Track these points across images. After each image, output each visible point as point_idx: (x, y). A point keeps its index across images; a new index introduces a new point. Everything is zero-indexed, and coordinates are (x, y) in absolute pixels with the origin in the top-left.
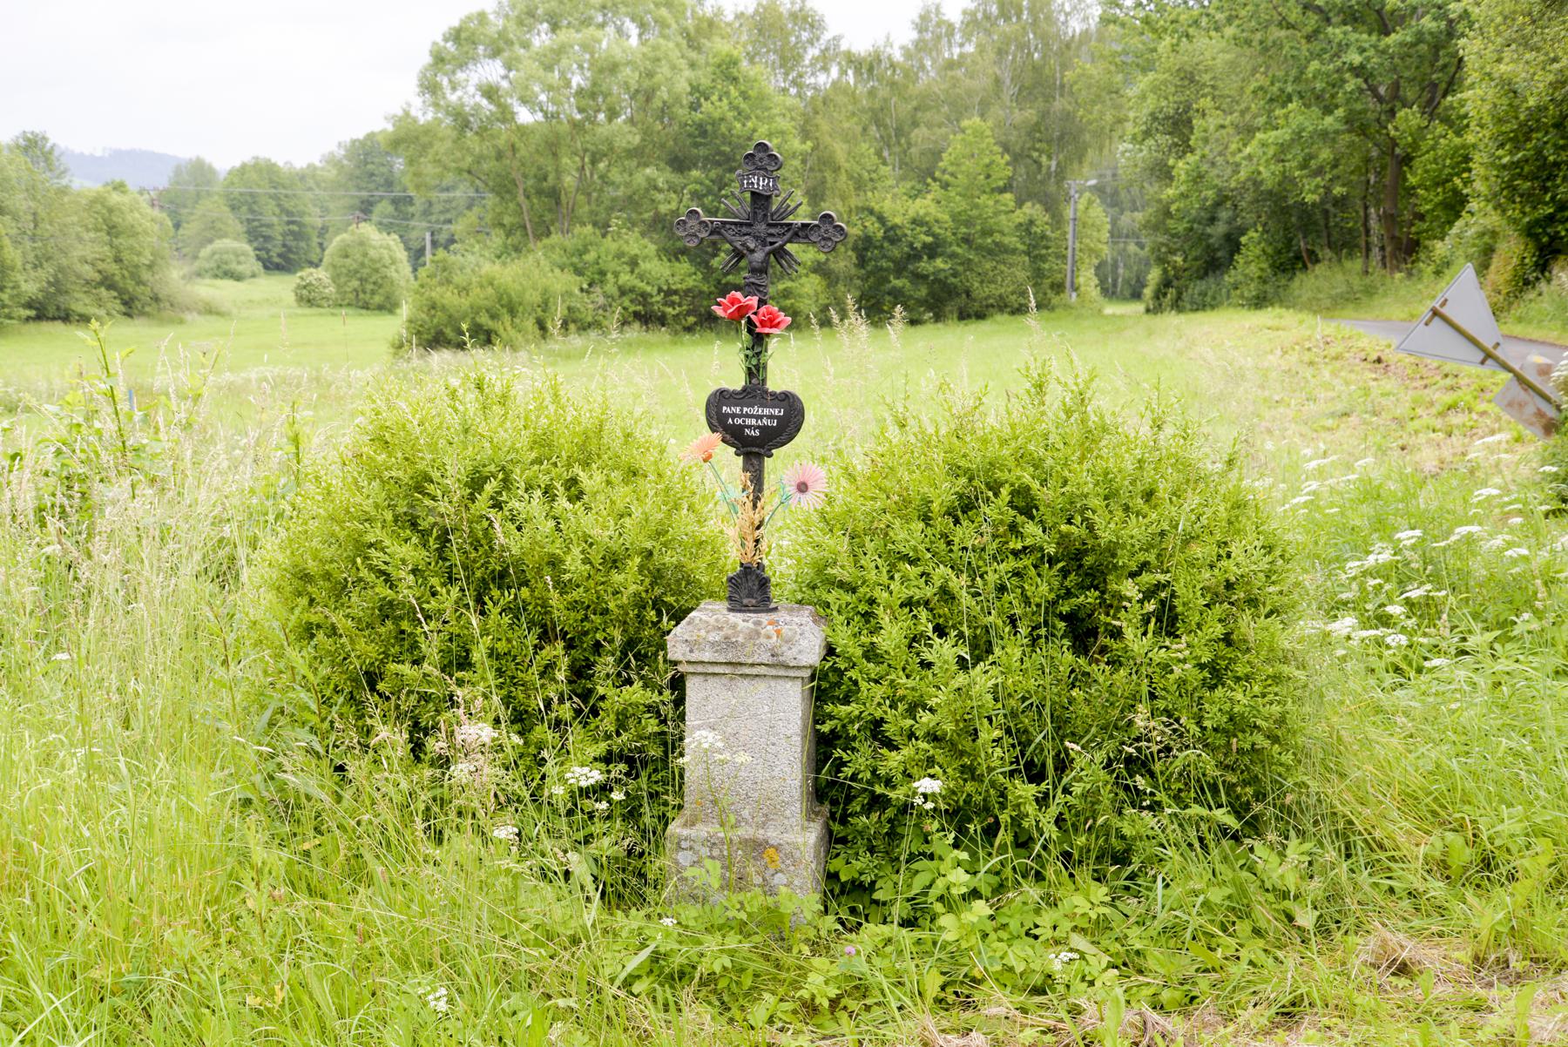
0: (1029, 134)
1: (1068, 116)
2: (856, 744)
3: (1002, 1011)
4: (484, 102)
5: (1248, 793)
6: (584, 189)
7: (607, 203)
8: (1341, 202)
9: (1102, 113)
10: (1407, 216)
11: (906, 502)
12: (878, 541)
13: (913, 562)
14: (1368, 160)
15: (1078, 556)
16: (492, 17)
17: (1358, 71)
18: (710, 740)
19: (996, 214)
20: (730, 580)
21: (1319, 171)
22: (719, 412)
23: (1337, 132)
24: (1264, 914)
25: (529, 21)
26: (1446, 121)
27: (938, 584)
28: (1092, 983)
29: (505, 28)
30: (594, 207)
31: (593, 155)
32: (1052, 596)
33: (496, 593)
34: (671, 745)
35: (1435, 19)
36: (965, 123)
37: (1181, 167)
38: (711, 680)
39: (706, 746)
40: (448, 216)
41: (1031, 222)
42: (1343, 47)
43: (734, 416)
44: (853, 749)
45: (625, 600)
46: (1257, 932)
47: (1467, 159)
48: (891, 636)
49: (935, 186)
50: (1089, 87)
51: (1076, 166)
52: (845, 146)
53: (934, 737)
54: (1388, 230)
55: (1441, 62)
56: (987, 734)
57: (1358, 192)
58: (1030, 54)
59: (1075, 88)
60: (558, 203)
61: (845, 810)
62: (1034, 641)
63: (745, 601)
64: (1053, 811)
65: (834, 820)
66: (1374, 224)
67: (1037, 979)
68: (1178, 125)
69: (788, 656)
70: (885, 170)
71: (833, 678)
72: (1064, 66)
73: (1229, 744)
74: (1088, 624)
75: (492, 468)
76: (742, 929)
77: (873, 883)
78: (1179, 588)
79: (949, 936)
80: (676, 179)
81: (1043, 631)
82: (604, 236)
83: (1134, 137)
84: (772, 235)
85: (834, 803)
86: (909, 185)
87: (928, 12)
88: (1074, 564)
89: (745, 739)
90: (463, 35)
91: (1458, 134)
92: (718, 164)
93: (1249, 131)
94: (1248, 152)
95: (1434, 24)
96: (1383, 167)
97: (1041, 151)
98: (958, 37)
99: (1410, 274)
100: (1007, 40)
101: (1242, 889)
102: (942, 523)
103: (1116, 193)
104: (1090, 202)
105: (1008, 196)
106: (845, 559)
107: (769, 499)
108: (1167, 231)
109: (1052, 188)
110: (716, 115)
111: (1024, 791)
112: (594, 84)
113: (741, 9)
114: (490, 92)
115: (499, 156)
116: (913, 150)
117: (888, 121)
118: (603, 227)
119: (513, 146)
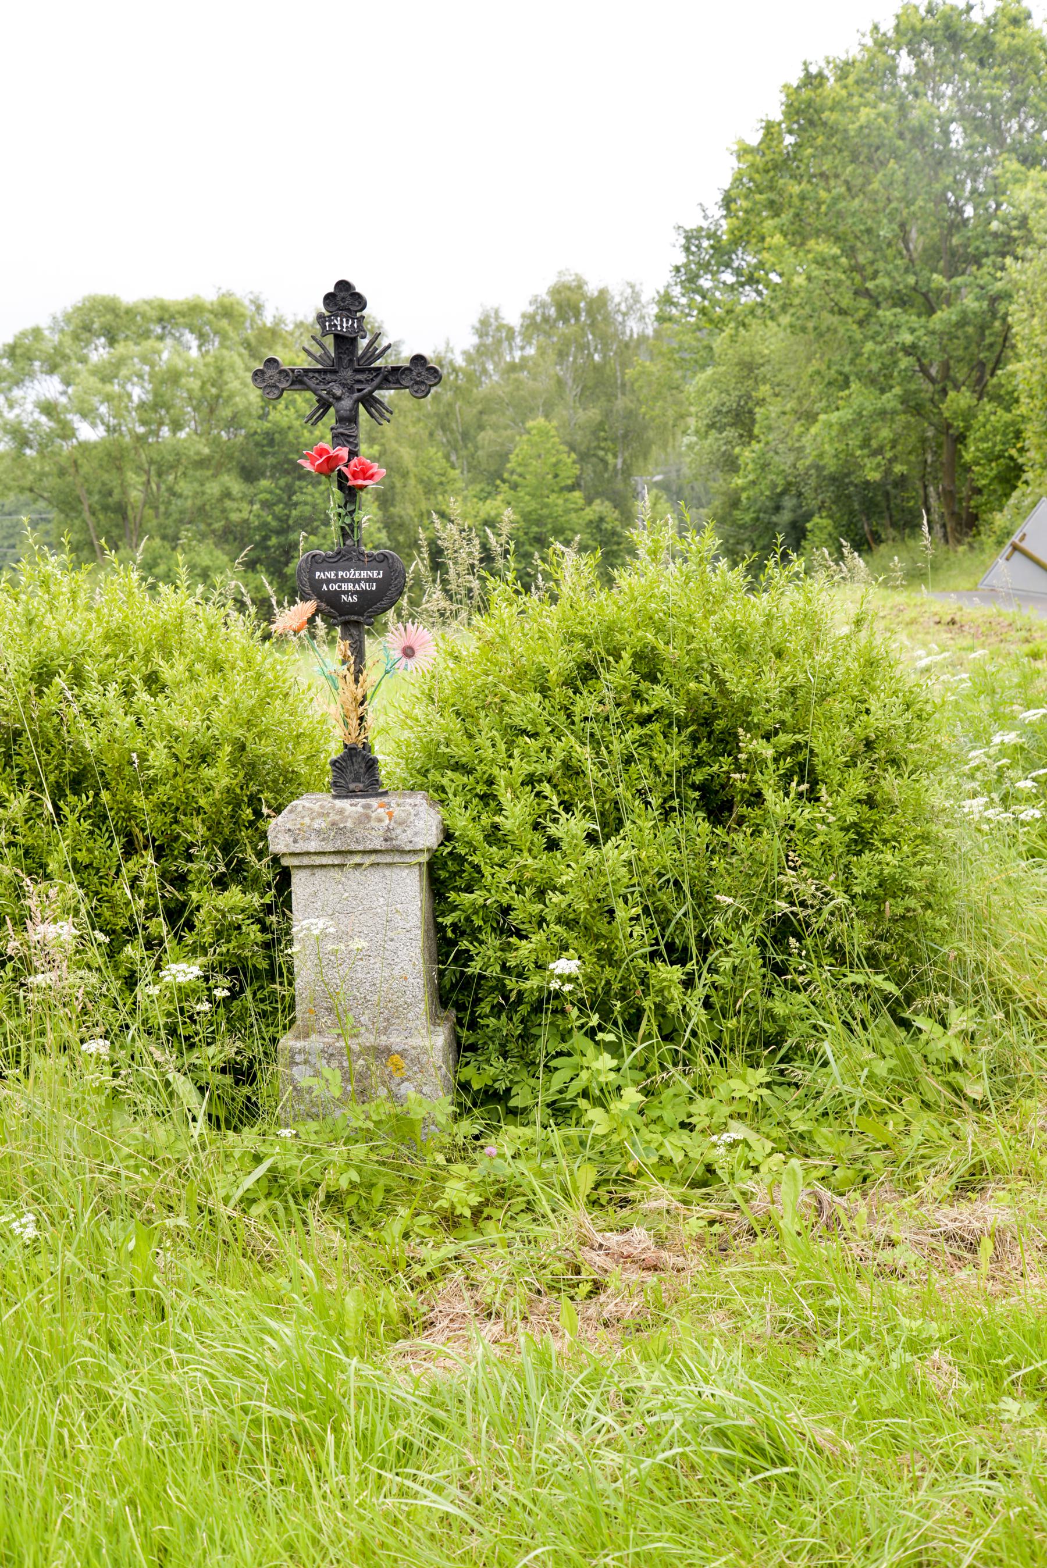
0: (594, 433)
1: (630, 414)
2: (482, 937)
3: (662, 1204)
4: (44, 419)
5: (902, 964)
6: (150, 501)
7: (176, 516)
8: (902, 482)
9: (664, 410)
10: (965, 491)
11: (521, 675)
12: (493, 717)
13: (535, 735)
14: (923, 440)
15: (707, 722)
16: (47, 333)
17: (910, 350)
18: (321, 926)
19: (567, 511)
20: (334, 763)
21: (879, 451)
22: (312, 579)
23: (894, 412)
24: (932, 1085)
25: (85, 335)
26: (997, 398)
27: (562, 756)
28: (756, 1169)
29: (61, 343)
30: (162, 519)
31: (160, 466)
32: (683, 763)
33: (72, 798)
34: (276, 940)
35: (977, 299)
36: (530, 424)
37: (747, 455)
38: (319, 873)
39: (316, 932)
40: (12, 541)
41: (601, 519)
42: (895, 328)
43: (328, 581)
44: (481, 942)
45: (217, 796)
46: (926, 1105)
47: (1018, 435)
48: (516, 812)
49: (505, 487)
50: (650, 384)
51: (641, 464)
52: (413, 452)
53: (570, 924)
54: (948, 506)
55: (987, 341)
56: (622, 913)
57: (916, 473)
58: (590, 356)
59: (637, 385)
60: (125, 517)
61: (473, 1012)
62: (667, 813)
63: (352, 786)
64: (700, 992)
65: (462, 1026)
66: (933, 502)
67: (697, 1170)
68: (741, 419)
69: (403, 839)
70: (455, 473)
71: (452, 867)
72: (624, 365)
73: (880, 912)
74: (722, 796)
75: (61, 661)
76: (368, 1136)
77: (508, 1090)
78: (817, 746)
79: (599, 1130)
80: (250, 490)
81: (675, 803)
82: (174, 549)
83: (697, 432)
84: (359, 381)
85: (460, 1007)
86: (478, 487)
87: (488, 317)
88: (705, 730)
89: (360, 935)
90: (18, 351)
91: (1008, 410)
92: (287, 472)
93: (811, 417)
94: (813, 437)
95: (976, 304)
96: (940, 446)
97: (606, 450)
98: (518, 340)
99: (971, 547)
100: (566, 342)
101: (906, 1060)
102: (560, 694)
103: (680, 489)
104: (657, 498)
105: (577, 494)
106: (459, 737)
107: (372, 673)
108: (734, 522)
109: (619, 485)
110: (284, 423)
111: (670, 974)
112: (156, 394)
113: (300, 318)
114: (48, 409)
115: (62, 473)
116: (480, 453)
117: (454, 425)
118: (172, 540)
119: (75, 462)
